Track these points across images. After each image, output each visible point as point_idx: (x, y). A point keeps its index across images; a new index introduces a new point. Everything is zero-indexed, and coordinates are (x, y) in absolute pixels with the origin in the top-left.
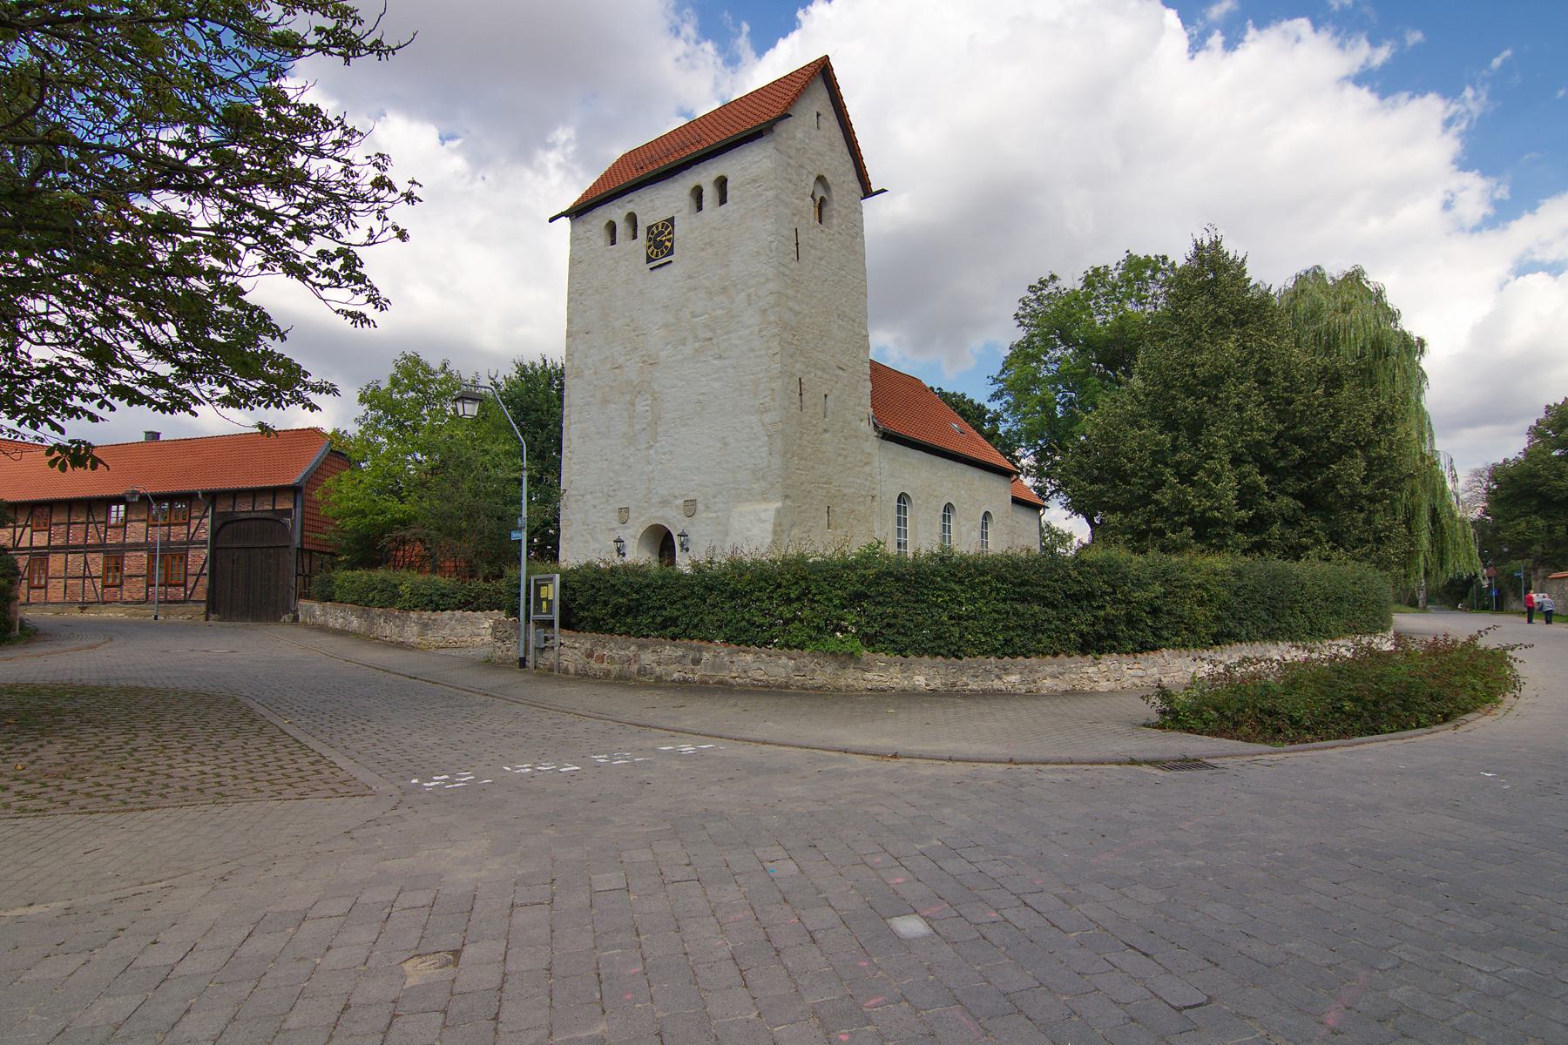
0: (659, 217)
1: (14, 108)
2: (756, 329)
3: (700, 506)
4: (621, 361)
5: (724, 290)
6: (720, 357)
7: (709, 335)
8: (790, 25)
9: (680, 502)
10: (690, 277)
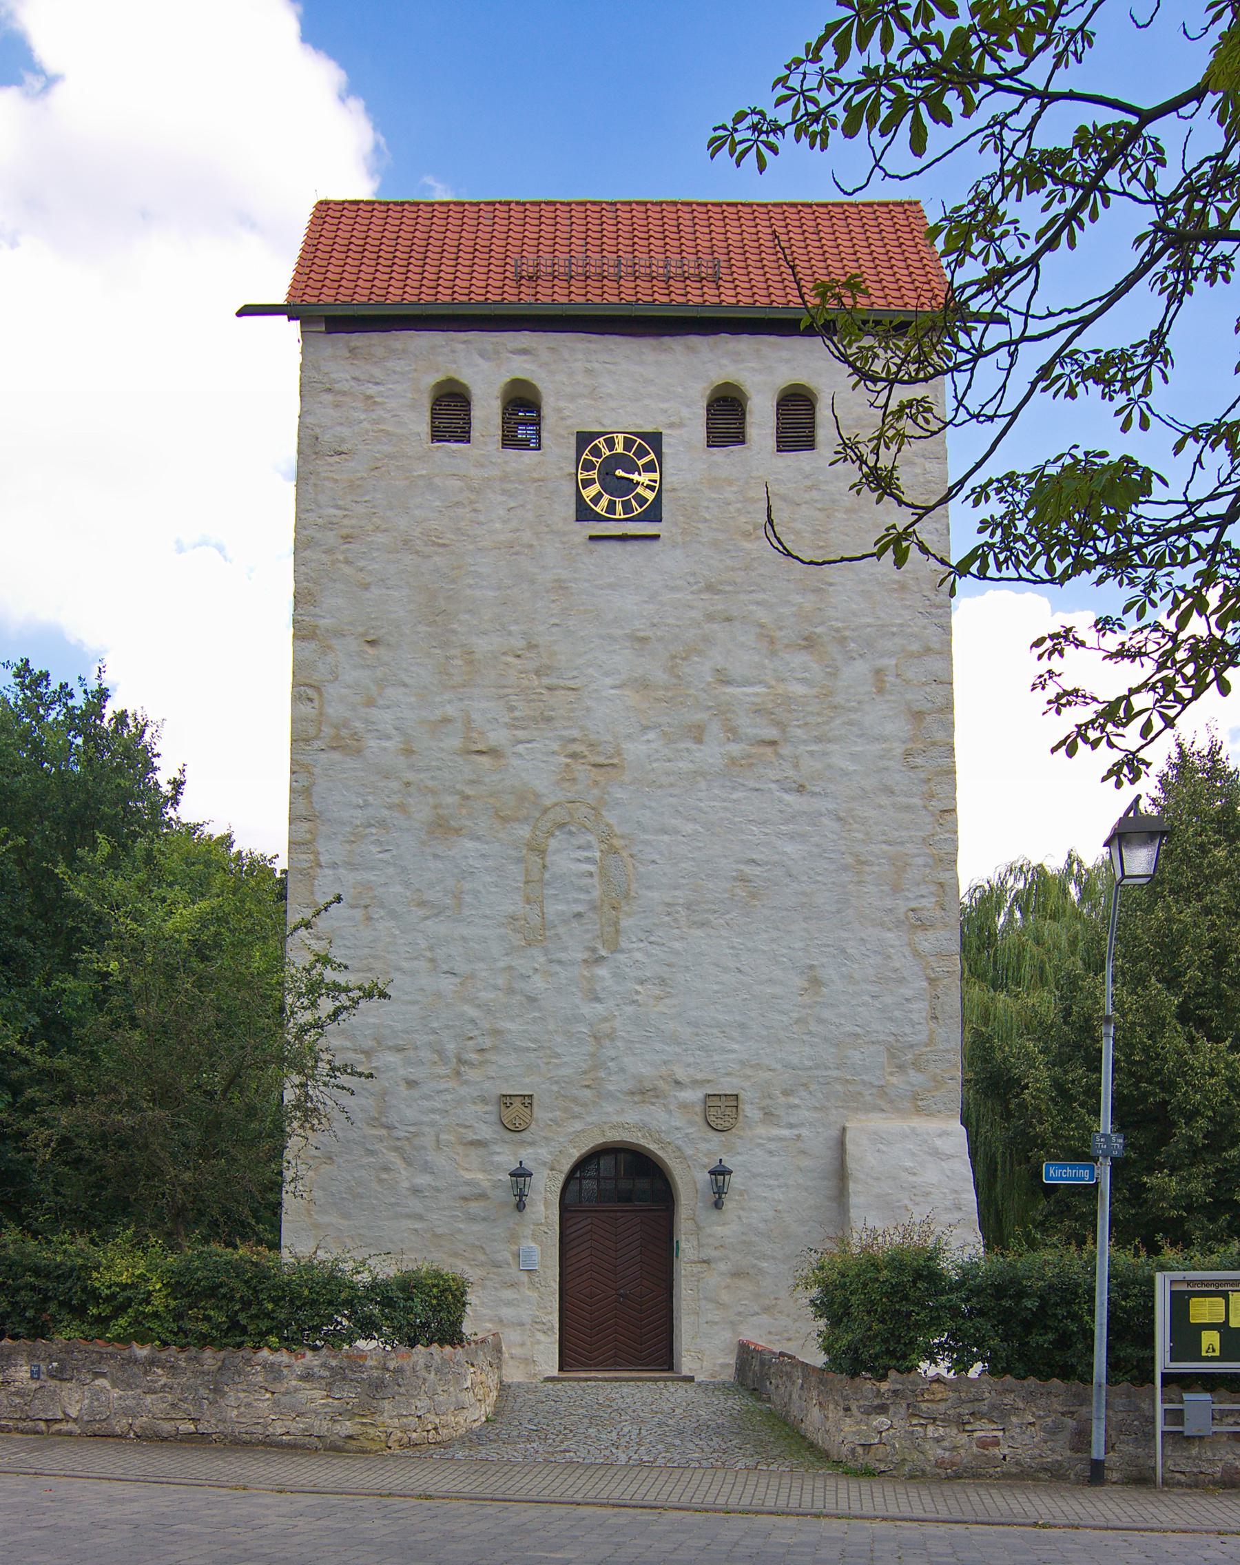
0: (620, 418)
1: (1239, 903)
2: (899, 749)
3: (750, 1111)
4: (497, 737)
5: (809, 643)
6: (801, 789)
7: (771, 733)
8: (1071, 611)
9: (693, 1095)
10: (710, 588)
